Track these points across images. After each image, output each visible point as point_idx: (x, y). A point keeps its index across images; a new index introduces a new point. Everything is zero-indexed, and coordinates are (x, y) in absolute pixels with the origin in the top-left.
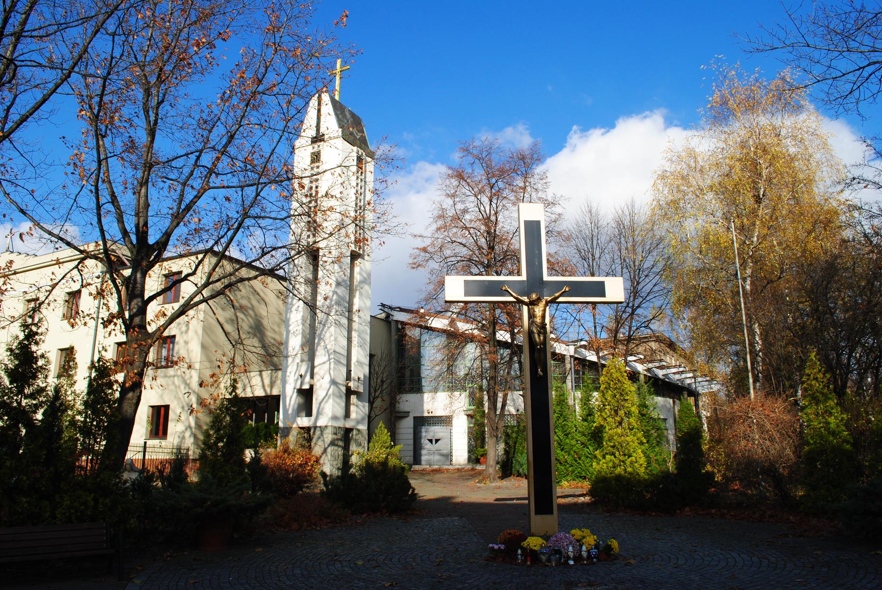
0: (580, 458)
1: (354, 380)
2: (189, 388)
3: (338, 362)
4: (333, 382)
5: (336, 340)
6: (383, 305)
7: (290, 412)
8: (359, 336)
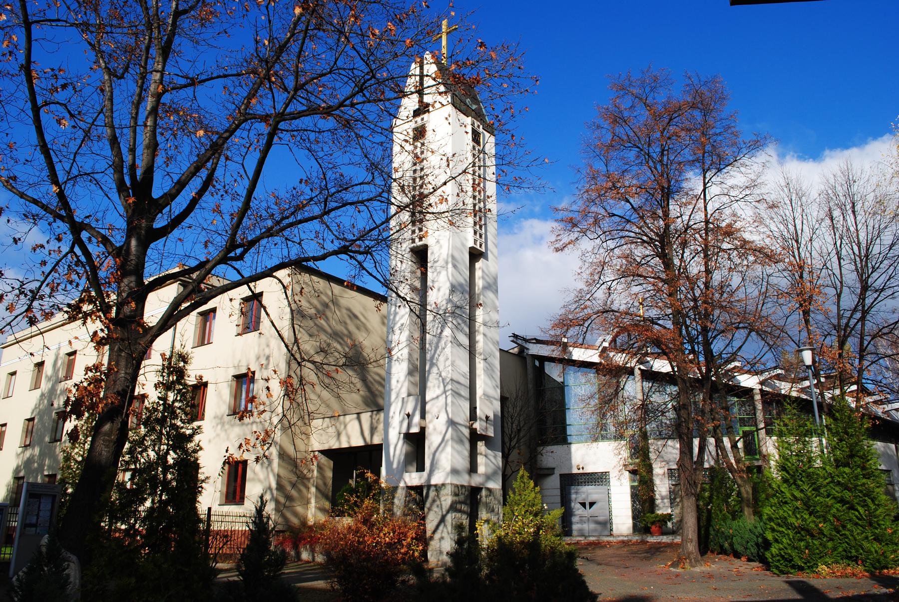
0: (844, 527)
1: (481, 419)
3: (456, 394)
4: (451, 423)
5: (453, 364)
6: (515, 336)
7: (395, 466)
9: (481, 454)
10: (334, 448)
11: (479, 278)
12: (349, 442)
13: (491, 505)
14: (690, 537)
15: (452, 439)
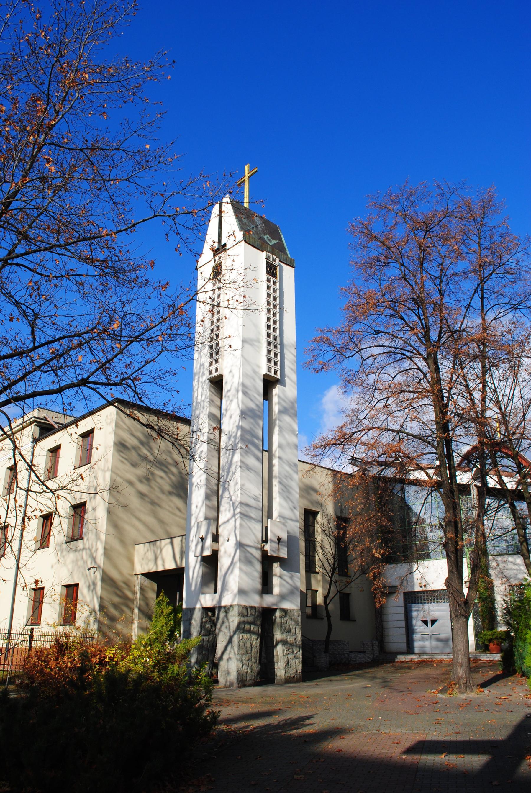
2: (95, 562)
4: (240, 545)
5: (242, 488)
7: (193, 588)
8: (280, 483)
9: (276, 575)
10: (152, 571)
11: (276, 404)
12: (164, 565)
13: (287, 626)
14: (460, 661)
15: (240, 560)
